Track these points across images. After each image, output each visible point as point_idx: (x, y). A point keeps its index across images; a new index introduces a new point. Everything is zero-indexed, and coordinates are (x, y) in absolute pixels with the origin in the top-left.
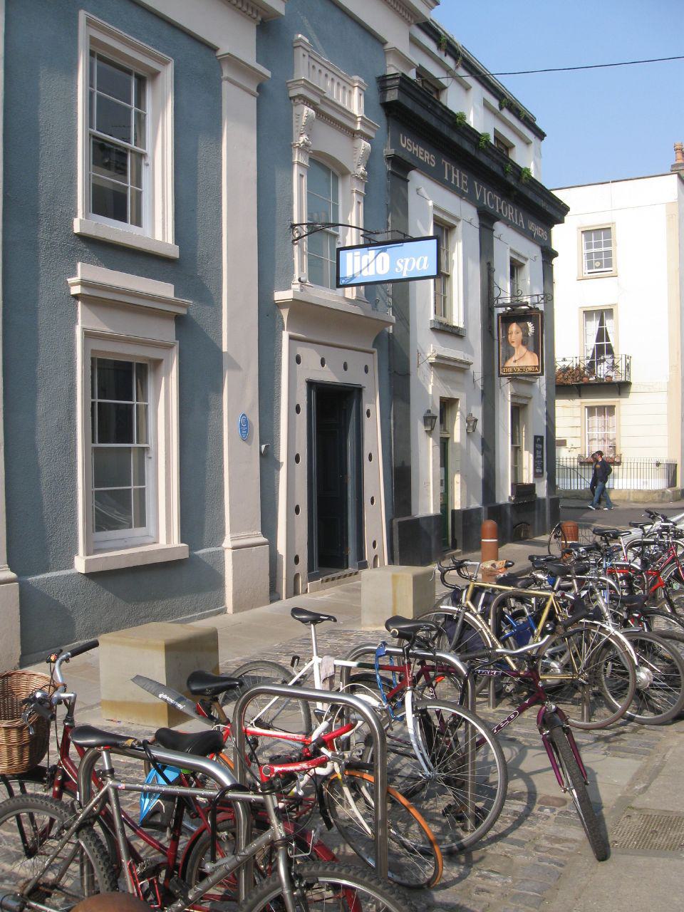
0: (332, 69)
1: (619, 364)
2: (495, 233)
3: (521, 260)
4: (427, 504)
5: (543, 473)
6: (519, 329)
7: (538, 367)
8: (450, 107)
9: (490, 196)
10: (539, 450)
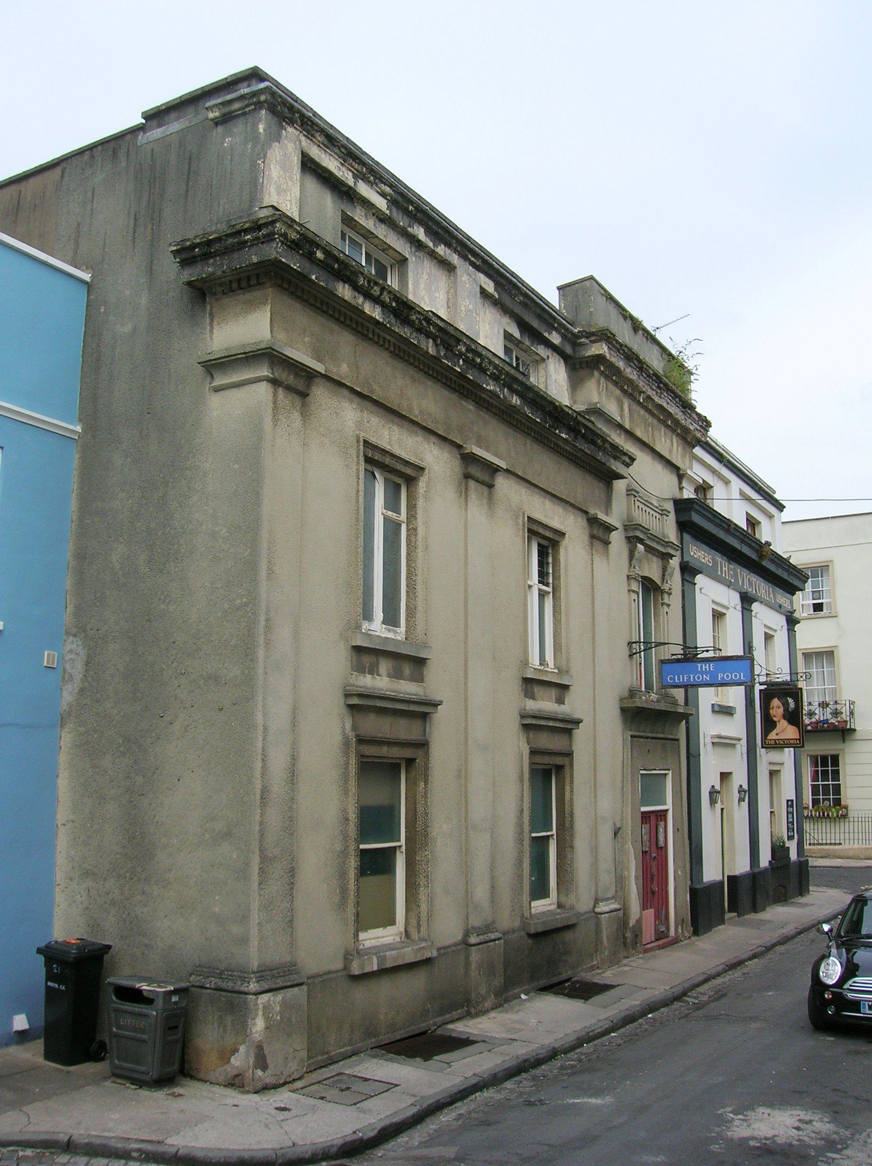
0: (649, 505)
1: (843, 710)
2: (753, 613)
3: (771, 633)
4: (711, 873)
5: (794, 835)
6: (781, 705)
7: (799, 740)
8: (715, 508)
9: (749, 579)
10: (791, 813)
